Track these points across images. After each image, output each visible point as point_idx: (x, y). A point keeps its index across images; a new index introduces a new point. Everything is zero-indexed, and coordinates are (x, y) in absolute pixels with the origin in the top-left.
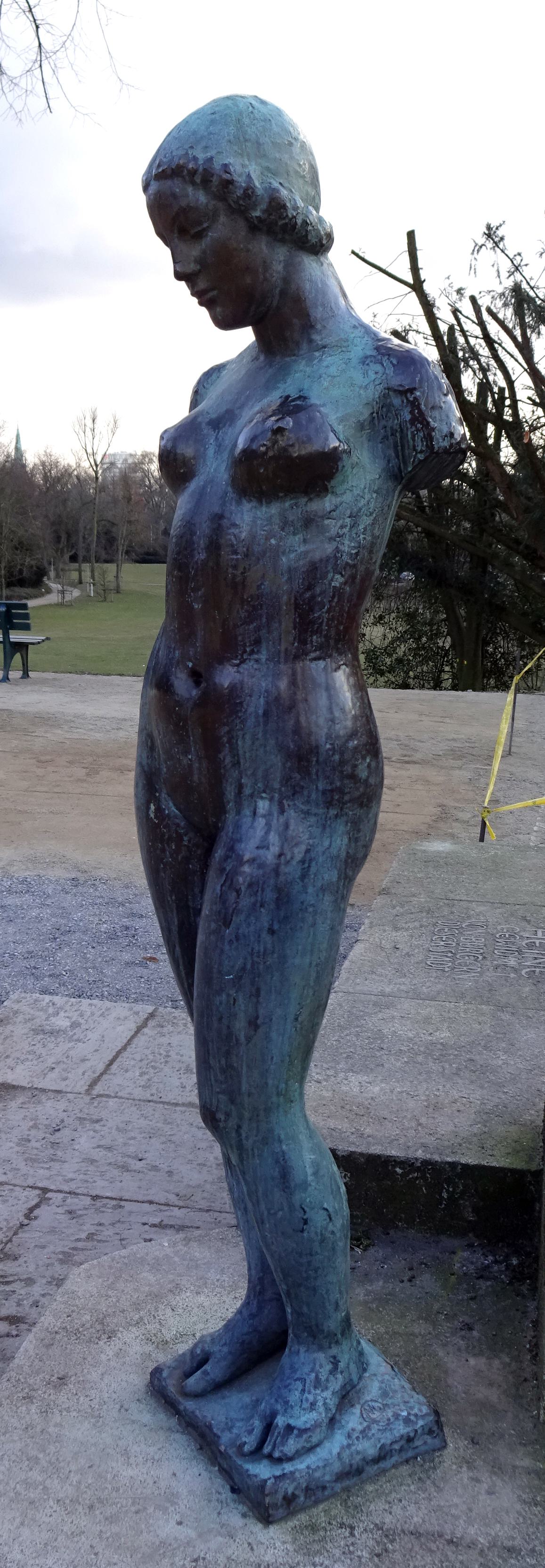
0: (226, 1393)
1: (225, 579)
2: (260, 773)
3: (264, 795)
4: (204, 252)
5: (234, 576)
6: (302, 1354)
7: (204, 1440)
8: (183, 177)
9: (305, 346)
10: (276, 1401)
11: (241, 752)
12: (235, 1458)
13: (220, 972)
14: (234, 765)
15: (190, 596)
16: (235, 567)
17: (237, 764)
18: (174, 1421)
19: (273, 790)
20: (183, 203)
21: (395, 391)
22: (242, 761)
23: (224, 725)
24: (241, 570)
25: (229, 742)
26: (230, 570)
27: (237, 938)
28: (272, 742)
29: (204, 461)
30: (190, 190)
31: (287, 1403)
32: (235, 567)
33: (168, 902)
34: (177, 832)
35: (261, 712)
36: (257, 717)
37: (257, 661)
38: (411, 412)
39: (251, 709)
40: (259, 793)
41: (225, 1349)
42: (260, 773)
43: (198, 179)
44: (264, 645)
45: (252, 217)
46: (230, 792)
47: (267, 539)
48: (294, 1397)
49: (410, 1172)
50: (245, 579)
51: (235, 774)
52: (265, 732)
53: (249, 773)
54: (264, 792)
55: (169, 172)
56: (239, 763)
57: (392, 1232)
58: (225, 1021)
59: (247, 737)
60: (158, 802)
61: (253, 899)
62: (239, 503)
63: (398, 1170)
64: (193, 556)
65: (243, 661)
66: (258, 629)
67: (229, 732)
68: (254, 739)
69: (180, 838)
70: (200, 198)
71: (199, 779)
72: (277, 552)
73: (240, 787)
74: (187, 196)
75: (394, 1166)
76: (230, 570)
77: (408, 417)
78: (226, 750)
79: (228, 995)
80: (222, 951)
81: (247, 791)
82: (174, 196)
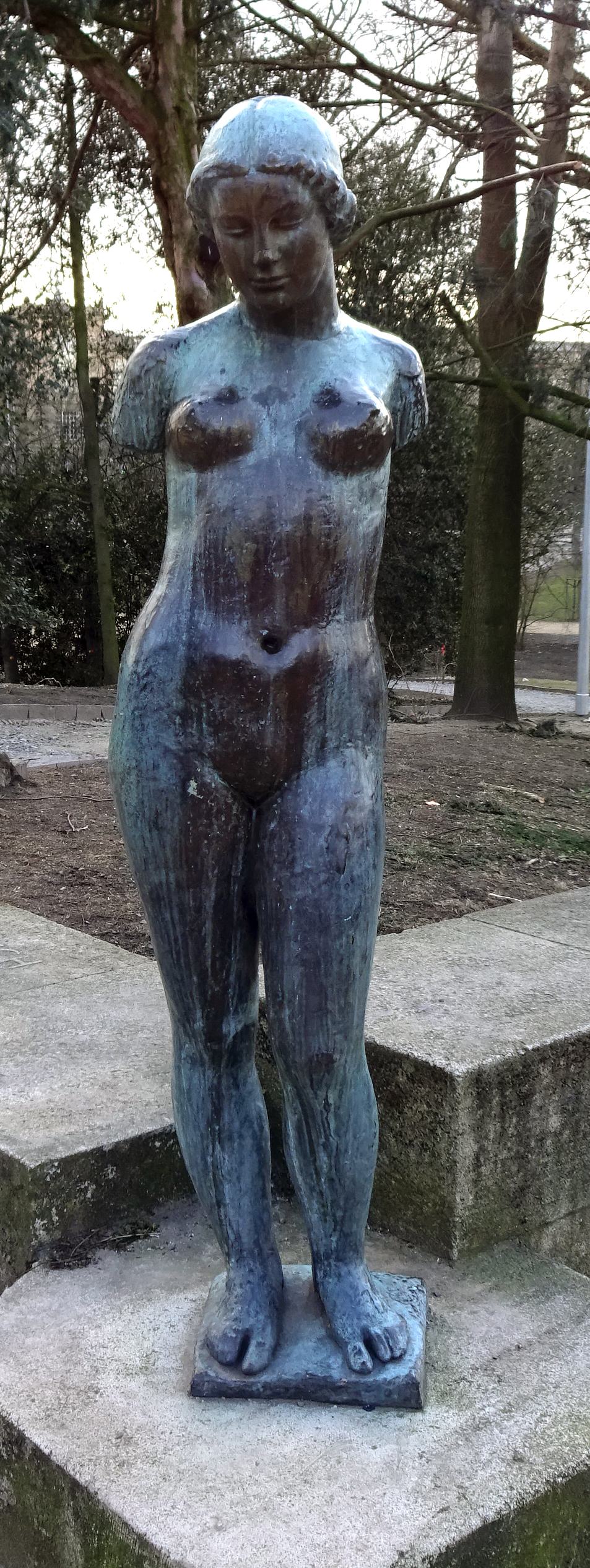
0: (283, 1352)
1: (318, 547)
2: (345, 725)
3: (349, 744)
4: (292, 243)
5: (327, 545)
6: (354, 1272)
7: (311, 1393)
8: (299, 177)
9: (327, 331)
10: (358, 1319)
11: (328, 708)
12: (362, 1380)
13: (338, 917)
14: (319, 721)
15: (270, 566)
16: (328, 536)
17: (322, 720)
18: (253, 1405)
19: (357, 738)
20: (294, 198)
21: (405, 377)
22: (328, 716)
23: (317, 684)
24: (333, 538)
25: (319, 700)
26: (323, 539)
27: (352, 881)
28: (355, 694)
29: (262, 434)
30: (300, 188)
31: (368, 1315)
32: (328, 536)
33: (208, 877)
34: (226, 803)
35: (346, 668)
36: (344, 673)
37: (338, 621)
38: (416, 396)
39: (339, 667)
40: (345, 742)
41: (261, 1317)
42: (345, 725)
43: (312, 181)
44: (342, 606)
45: (335, 219)
46: (311, 747)
47: (351, 509)
48: (369, 1308)
49: (167, 1141)
50: (336, 547)
51: (319, 730)
52: (349, 685)
53: (334, 726)
54: (350, 741)
55: (286, 169)
56: (325, 719)
57: (155, 1211)
58: (345, 962)
59: (335, 693)
60: (198, 777)
61: (360, 842)
62: (326, 478)
63: (158, 1144)
64: (274, 528)
65: (328, 623)
66: (341, 592)
67: (321, 690)
68: (341, 694)
69: (229, 807)
70: (304, 196)
71: (274, 742)
72: (357, 520)
73: (323, 742)
74: (297, 193)
75: (153, 1142)
76: (323, 539)
77: (413, 400)
78: (314, 709)
79: (348, 936)
80: (339, 897)
81: (332, 745)
82: (286, 191)
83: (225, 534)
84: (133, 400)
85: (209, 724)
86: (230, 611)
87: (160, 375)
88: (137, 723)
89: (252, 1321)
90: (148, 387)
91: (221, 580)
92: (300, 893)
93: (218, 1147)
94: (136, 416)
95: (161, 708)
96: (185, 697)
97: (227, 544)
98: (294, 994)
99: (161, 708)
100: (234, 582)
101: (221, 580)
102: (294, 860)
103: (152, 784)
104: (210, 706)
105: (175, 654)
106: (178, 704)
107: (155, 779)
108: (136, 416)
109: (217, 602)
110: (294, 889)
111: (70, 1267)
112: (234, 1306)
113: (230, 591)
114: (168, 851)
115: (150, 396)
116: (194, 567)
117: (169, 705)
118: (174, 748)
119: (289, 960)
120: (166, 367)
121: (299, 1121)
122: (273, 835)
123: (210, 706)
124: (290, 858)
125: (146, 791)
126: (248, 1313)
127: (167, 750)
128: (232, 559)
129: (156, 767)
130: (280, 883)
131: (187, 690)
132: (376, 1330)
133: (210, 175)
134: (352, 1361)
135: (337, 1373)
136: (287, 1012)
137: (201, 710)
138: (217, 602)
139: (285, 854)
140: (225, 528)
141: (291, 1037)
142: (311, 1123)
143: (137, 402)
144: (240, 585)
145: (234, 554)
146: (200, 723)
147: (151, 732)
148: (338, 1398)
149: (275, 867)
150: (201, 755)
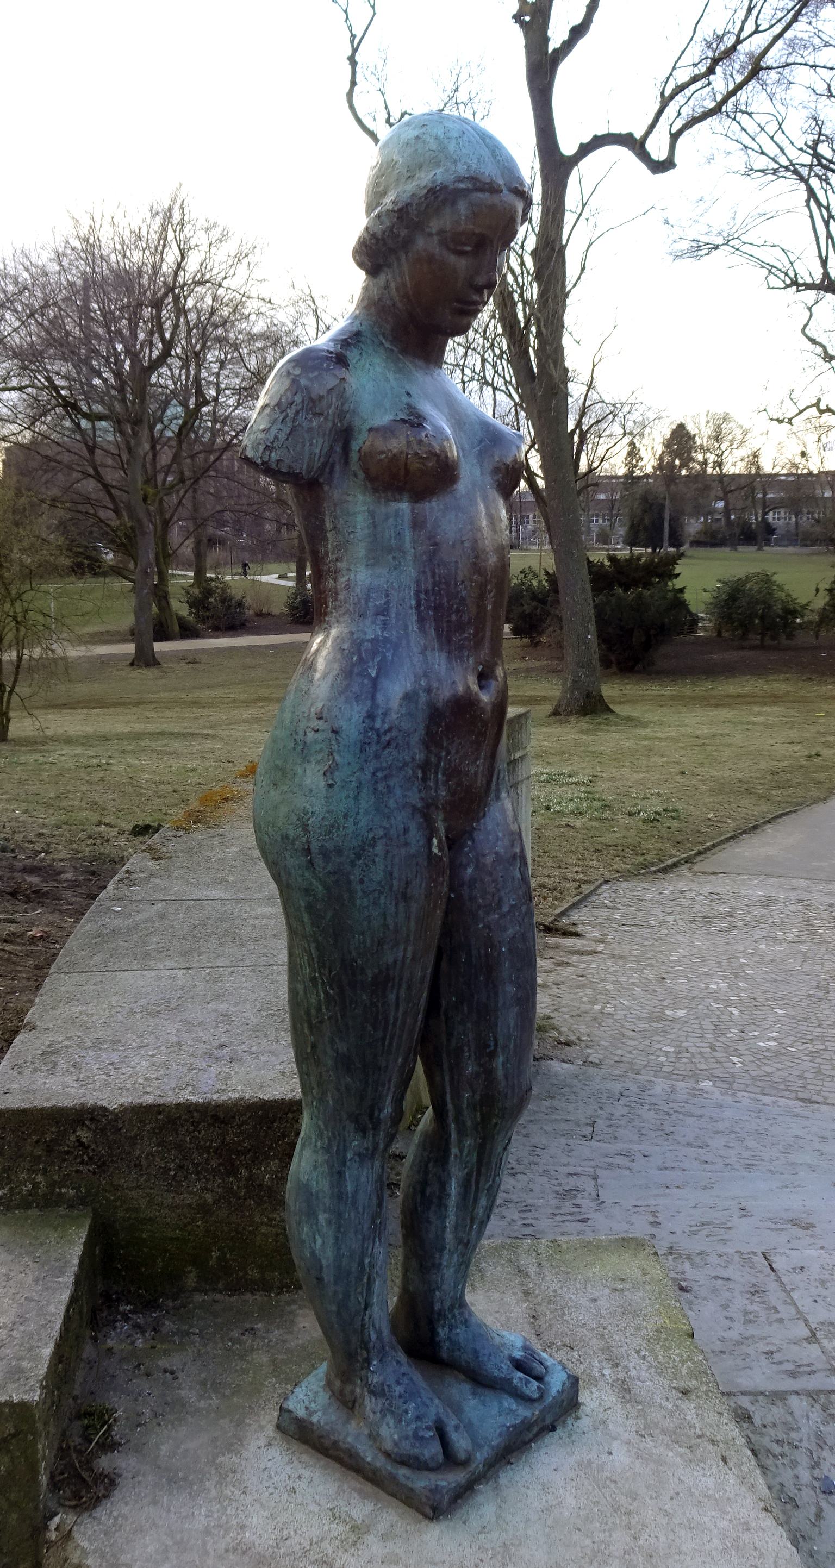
83: (457, 568)
84: (311, 421)
85: (443, 774)
86: (461, 648)
87: (342, 396)
88: (381, 787)
89: (433, 1411)
90: (329, 407)
91: (454, 617)
92: (510, 932)
93: (377, 1243)
94: (311, 440)
95: (406, 764)
96: (427, 748)
97: (460, 578)
98: (509, 1038)
99: (406, 764)
100: (465, 618)
101: (454, 617)
102: (500, 900)
103: (403, 851)
104: (448, 753)
105: (417, 703)
106: (420, 756)
107: (406, 844)
108: (311, 440)
109: (449, 641)
110: (505, 929)
111: (106, 1497)
112: (405, 1407)
113: (461, 627)
114: (412, 923)
115: (330, 418)
116: (418, 605)
117: (413, 759)
118: (419, 805)
119: (504, 1003)
120: (346, 386)
121: (469, 1175)
122: (473, 881)
123: (448, 753)
124: (496, 899)
125: (397, 860)
126: (425, 1404)
127: (414, 808)
128: (464, 593)
129: (406, 830)
130: (490, 928)
131: (431, 740)
132: (518, 1354)
133: (462, 186)
134: (528, 1392)
135: (524, 1412)
136: (501, 1059)
137: (439, 759)
138: (449, 641)
139: (489, 897)
140: (456, 562)
141: (503, 1084)
142: (483, 1170)
143: (315, 424)
144: (469, 622)
145: (465, 588)
146: (436, 773)
147: (398, 792)
148: (531, 1435)
149: (481, 913)
150: (437, 808)
